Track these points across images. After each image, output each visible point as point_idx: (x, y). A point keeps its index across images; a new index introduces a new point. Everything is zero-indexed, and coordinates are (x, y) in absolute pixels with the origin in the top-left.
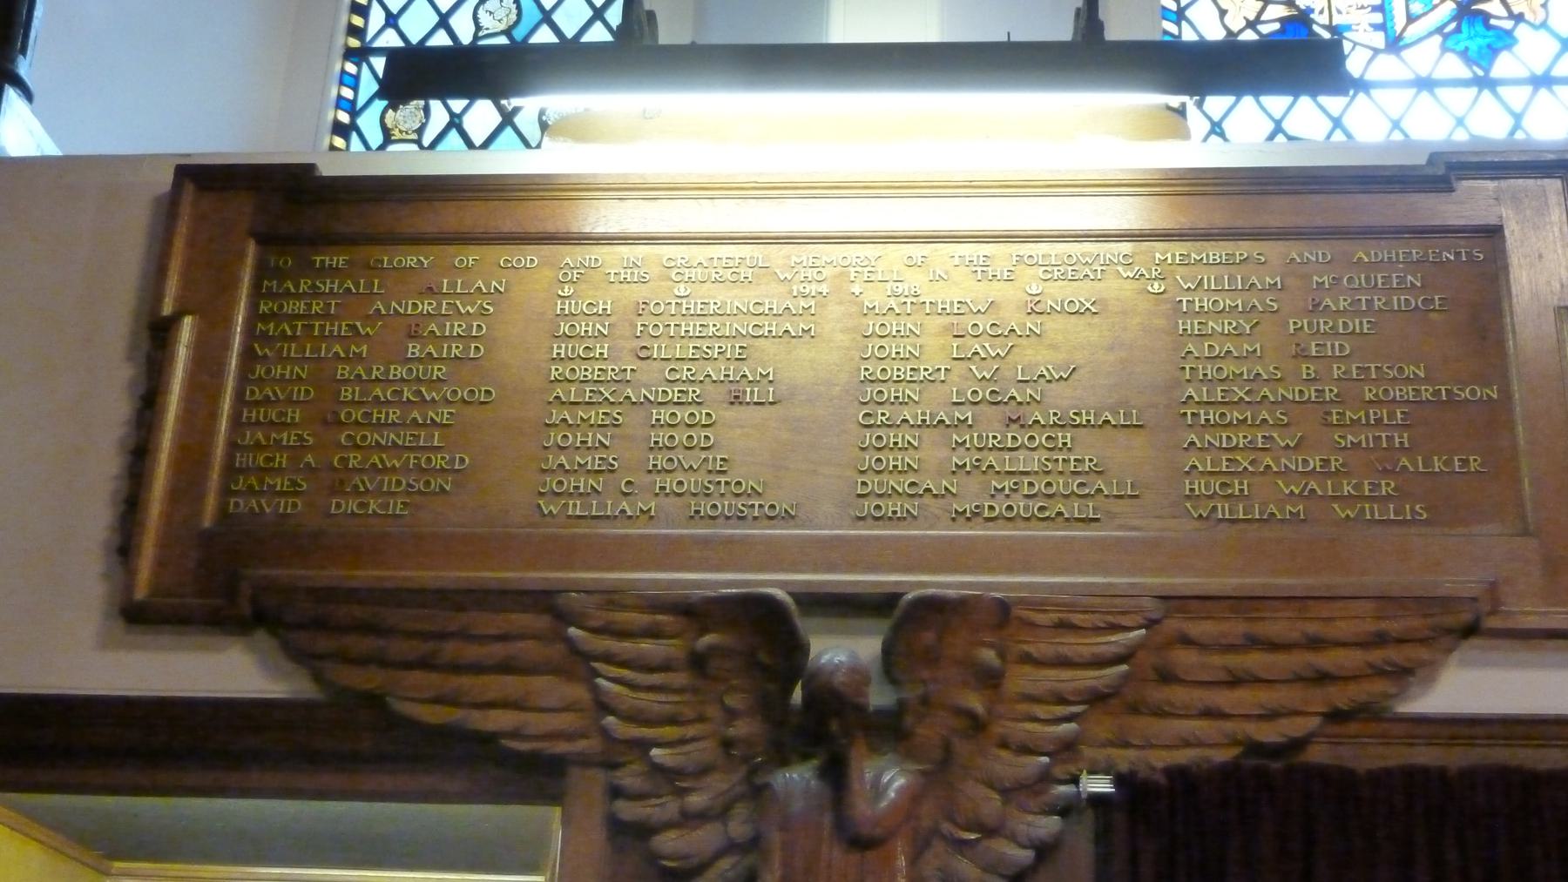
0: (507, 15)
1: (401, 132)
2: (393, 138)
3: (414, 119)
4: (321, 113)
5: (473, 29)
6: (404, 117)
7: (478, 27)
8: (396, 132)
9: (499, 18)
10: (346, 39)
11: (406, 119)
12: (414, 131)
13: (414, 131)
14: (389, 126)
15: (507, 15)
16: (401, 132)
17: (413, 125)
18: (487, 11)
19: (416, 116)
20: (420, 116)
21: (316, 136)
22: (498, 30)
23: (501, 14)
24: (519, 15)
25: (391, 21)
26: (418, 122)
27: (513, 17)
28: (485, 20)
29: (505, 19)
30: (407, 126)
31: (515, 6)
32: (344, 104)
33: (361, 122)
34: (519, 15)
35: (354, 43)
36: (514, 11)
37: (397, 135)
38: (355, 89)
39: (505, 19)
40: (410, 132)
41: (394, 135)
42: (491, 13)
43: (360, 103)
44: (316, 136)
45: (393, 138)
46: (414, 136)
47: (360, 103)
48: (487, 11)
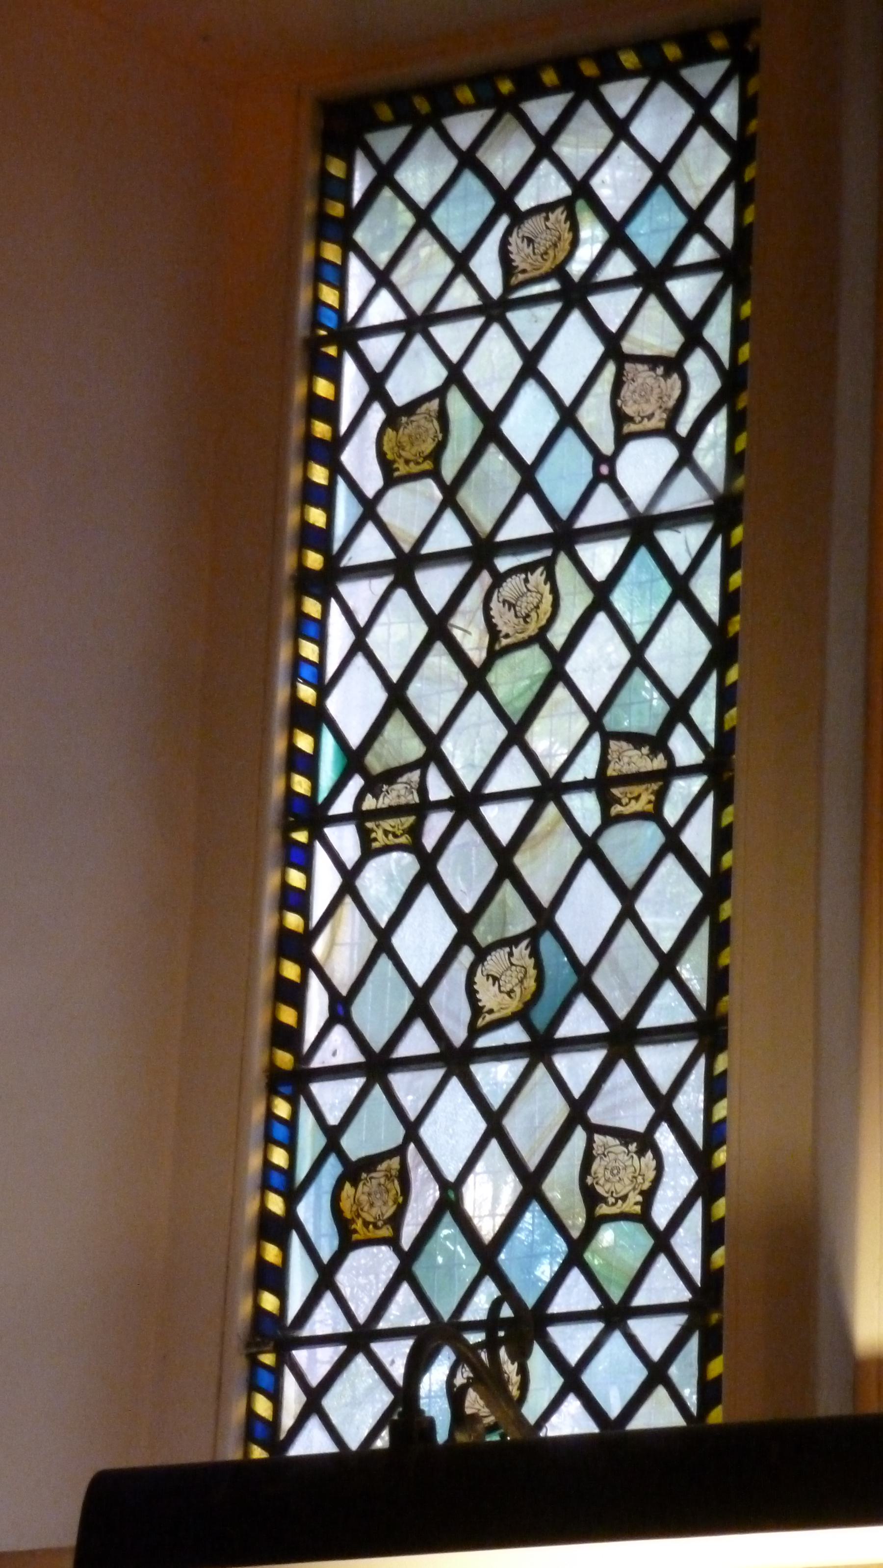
0: (521, 982)
1: (407, 462)
2: (355, 1237)
3: (385, 1196)
4: (235, 1204)
5: (466, 1013)
6: (369, 1194)
7: (477, 1010)
8: (358, 1225)
9: (508, 987)
10: (281, 919)
11: (373, 1198)
12: (425, 458)
13: (425, 458)
14: (348, 1215)
15: (521, 982)
16: (366, 1224)
17: (384, 1209)
18: (488, 976)
19: (388, 1191)
20: (394, 1192)
21: (231, 1225)
22: (507, 1012)
23: (510, 981)
24: (540, 979)
25: (340, 1009)
26: (391, 1203)
27: (531, 984)
28: (488, 996)
29: (518, 990)
30: (375, 1211)
31: (532, 961)
32: (312, 630)
33: (303, 1210)
34: (540, 979)
35: (285, 1059)
36: (532, 972)
37: (402, 469)
38: (291, 1148)
39: (518, 990)
40: (380, 1223)
41: (375, 840)
42: (495, 979)
43: (331, 668)
44: (231, 1225)
45: (355, 1237)
46: (427, 466)
47: (331, 668)
48: (488, 976)
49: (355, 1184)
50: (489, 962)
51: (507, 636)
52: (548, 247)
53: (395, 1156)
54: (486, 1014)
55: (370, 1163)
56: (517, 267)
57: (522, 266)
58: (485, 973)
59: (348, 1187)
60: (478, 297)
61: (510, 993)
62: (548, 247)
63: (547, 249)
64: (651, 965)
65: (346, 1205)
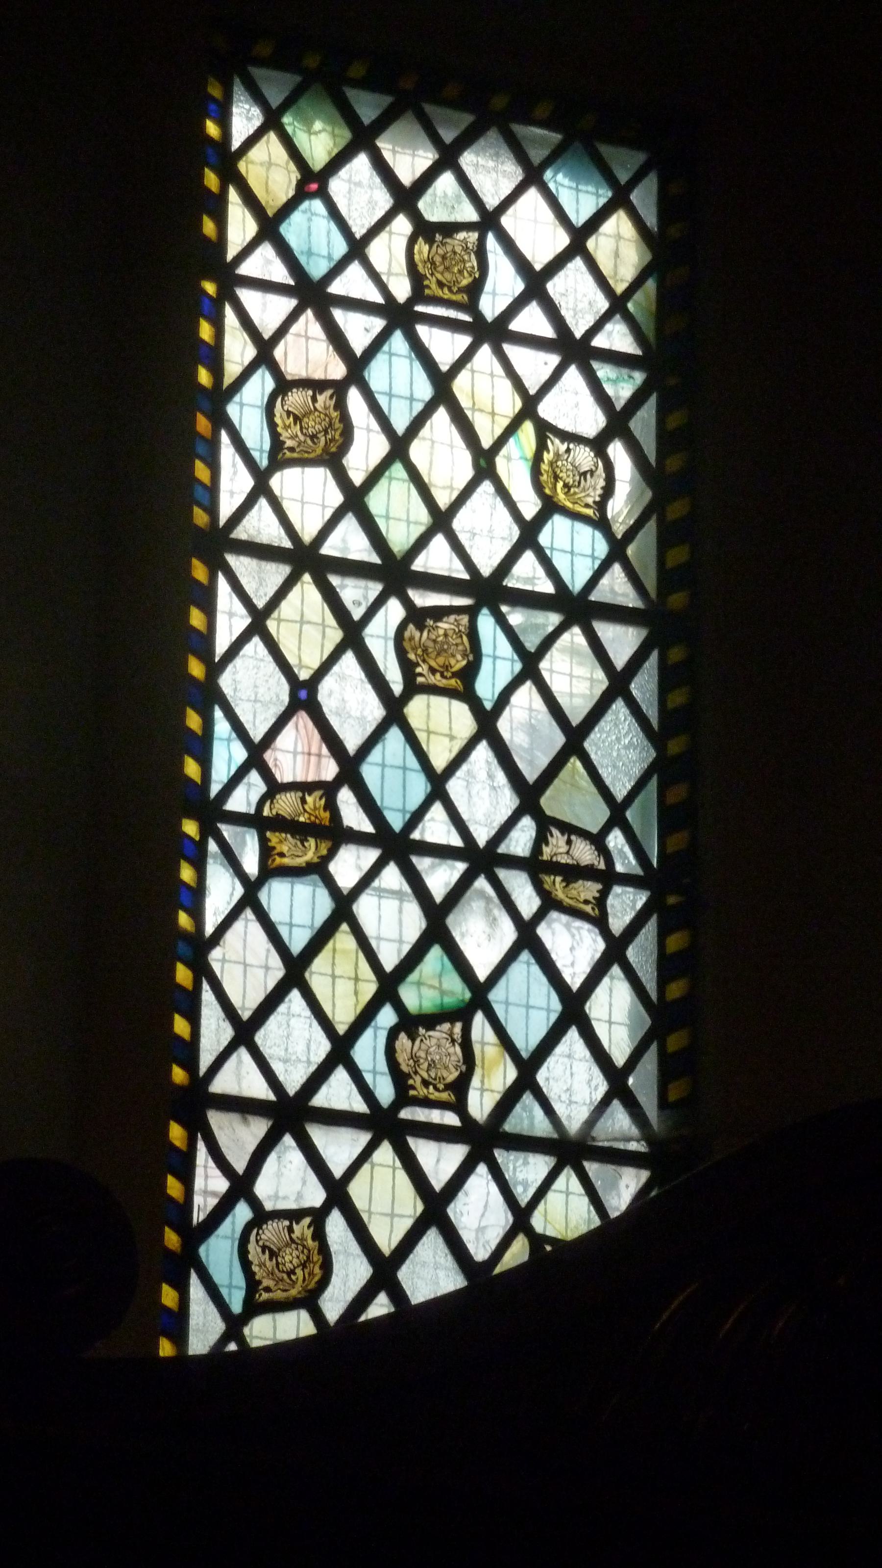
8: (416, 1081)
14: (404, 1068)
41: (428, 287)
49: (412, 1037)
50: (293, 395)
51: (268, 1289)
52: (296, 1265)
53: (537, 781)
54: (276, 857)
55: (431, 1020)
56: (274, 848)
57: (266, 1283)
58: (261, 1243)
59: (403, 1040)
60: (560, 200)
61: (313, 437)
62: (296, 1265)
63: (295, 1268)
64: (322, 1047)
65: (402, 1058)
